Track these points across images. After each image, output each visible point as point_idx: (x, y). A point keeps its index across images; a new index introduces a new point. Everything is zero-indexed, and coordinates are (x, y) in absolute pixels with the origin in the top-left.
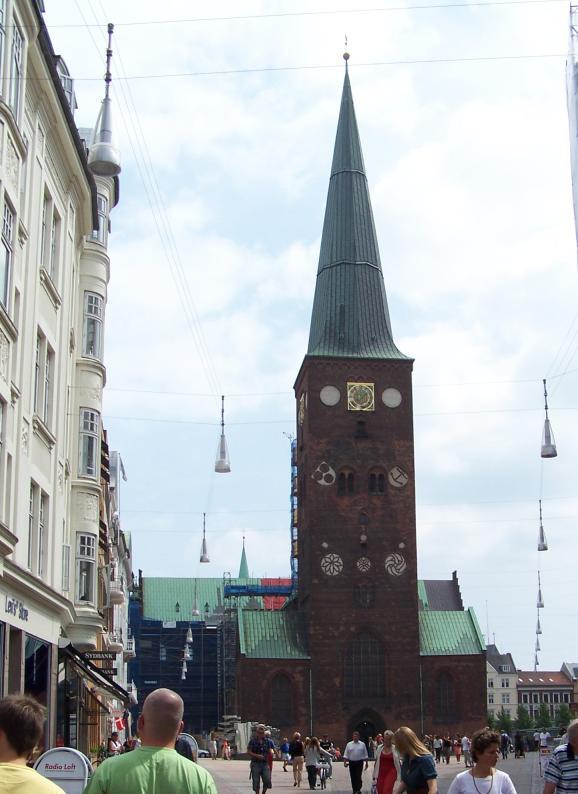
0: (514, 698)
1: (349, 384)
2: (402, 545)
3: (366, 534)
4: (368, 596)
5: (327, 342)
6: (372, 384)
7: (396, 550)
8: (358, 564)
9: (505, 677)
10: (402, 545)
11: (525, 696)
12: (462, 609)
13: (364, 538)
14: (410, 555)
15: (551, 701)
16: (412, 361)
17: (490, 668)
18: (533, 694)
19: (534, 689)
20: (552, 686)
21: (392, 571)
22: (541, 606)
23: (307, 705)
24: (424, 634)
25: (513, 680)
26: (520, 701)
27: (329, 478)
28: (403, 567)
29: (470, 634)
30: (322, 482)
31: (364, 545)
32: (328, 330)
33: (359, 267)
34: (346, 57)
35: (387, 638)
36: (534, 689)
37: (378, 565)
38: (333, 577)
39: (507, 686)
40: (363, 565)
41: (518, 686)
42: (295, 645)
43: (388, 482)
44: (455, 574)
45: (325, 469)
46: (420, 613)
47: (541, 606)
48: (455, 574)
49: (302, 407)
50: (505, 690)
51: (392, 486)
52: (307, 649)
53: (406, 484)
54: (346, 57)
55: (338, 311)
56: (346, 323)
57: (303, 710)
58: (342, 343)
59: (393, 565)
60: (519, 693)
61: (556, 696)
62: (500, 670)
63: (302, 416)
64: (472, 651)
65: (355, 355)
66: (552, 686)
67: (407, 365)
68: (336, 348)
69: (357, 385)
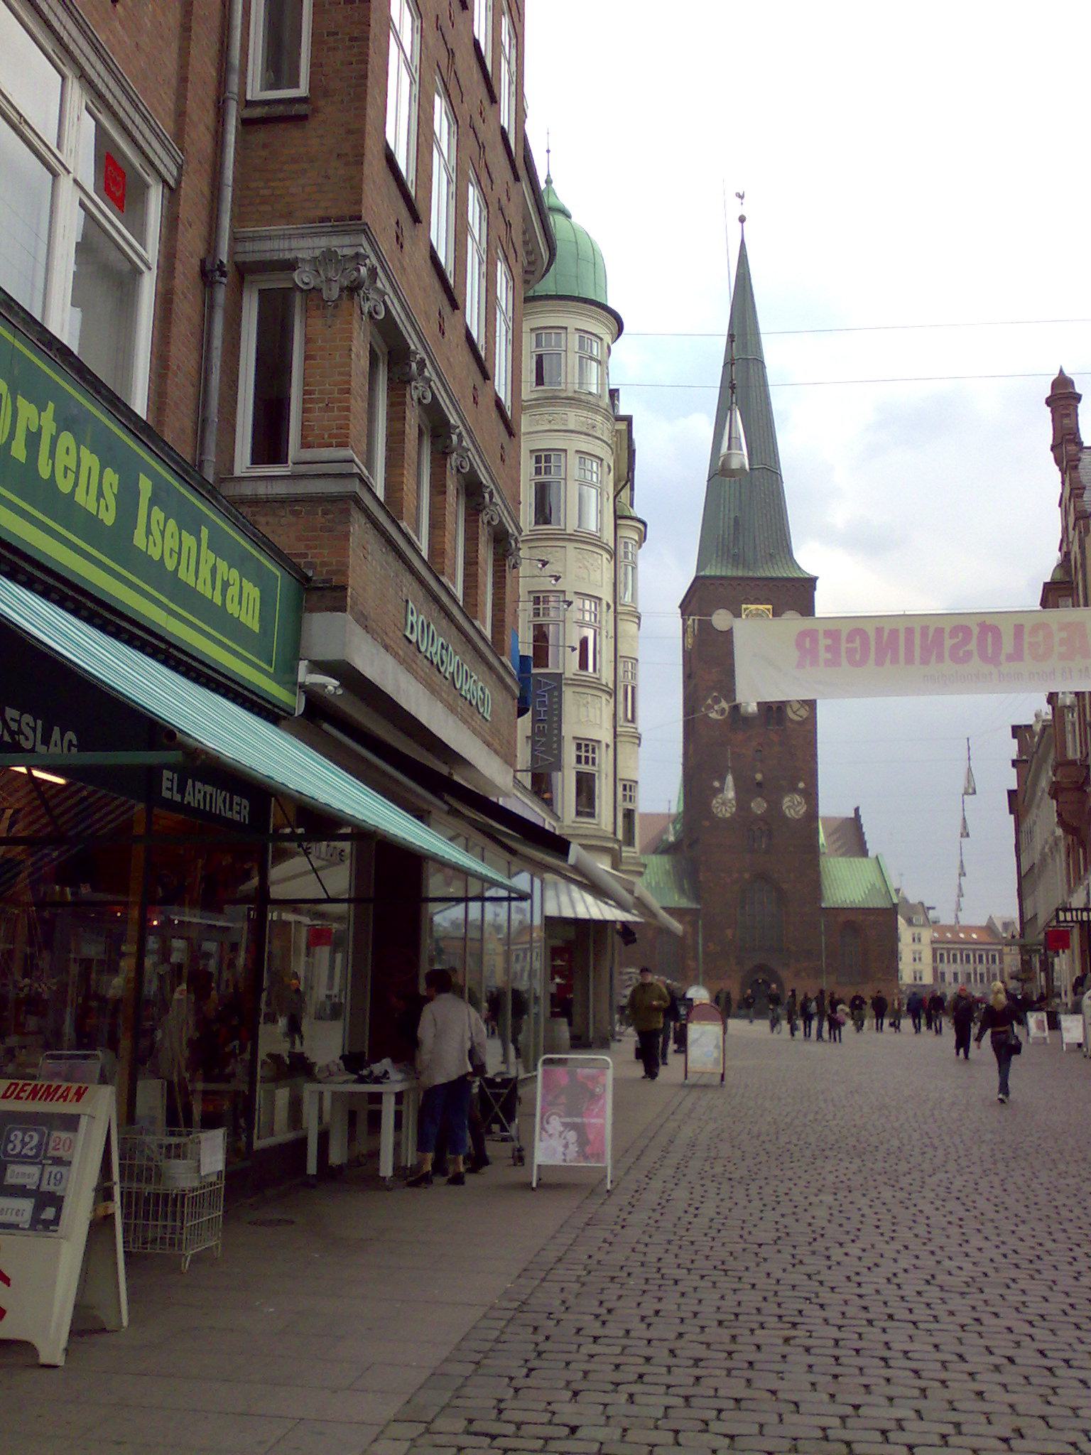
0: (927, 956)
1: (744, 606)
2: (801, 785)
3: (762, 772)
4: (764, 840)
5: (719, 559)
6: (770, 607)
7: (795, 790)
8: (752, 805)
9: (917, 930)
10: (801, 785)
11: (942, 955)
12: (864, 852)
13: (759, 777)
14: (811, 795)
15: (975, 962)
16: (816, 578)
17: (901, 921)
18: (977, 954)
19: (978, 947)
20: (949, 942)
21: (790, 813)
22: (966, 834)
23: (696, 958)
24: (826, 882)
25: (927, 935)
26: (934, 960)
27: (723, 711)
28: (802, 809)
29: (879, 884)
30: (713, 715)
31: (759, 784)
32: (720, 545)
33: (757, 472)
34: (742, 219)
35: (785, 886)
36: (978, 947)
37: (775, 806)
38: (724, 820)
39: (920, 959)
40: (758, 806)
41: (932, 942)
42: (682, 891)
43: (787, 714)
44: (857, 810)
45: (717, 701)
46: (822, 860)
47: (966, 834)
48: (857, 810)
49: (690, 630)
50: (917, 947)
51: (791, 720)
52: (697, 898)
53: (807, 718)
54: (742, 219)
55: (732, 523)
56: (741, 538)
57: (691, 963)
58: (736, 560)
59: (792, 806)
60: (934, 951)
61: (981, 957)
62: (910, 922)
63: (690, 641)
64: (879, 903)
65: (751, 574)
66: (949, 942)
67: (811, 582)
68: (730, 566)
69: (752, 607)
